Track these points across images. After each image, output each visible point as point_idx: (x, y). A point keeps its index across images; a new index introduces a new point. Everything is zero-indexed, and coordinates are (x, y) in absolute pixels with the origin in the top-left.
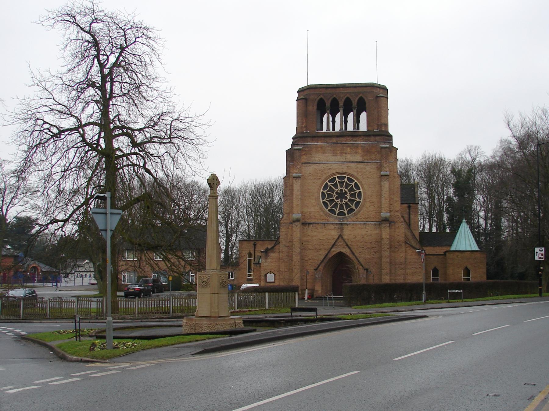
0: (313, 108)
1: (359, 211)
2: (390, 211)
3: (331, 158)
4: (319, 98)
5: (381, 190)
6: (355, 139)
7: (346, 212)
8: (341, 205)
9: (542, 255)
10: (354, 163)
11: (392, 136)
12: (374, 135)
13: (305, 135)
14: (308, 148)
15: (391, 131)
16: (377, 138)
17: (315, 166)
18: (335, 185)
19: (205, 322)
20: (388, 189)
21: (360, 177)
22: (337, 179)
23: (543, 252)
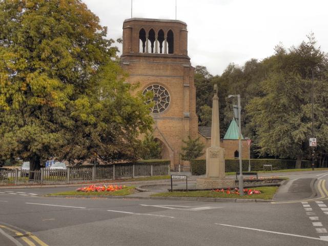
0: (136, 34)
1: (168, 110)
6: (166, 59)
9: (315, 143)
12: (179, 58)
13: (131, 54)
14: (133, 64)
15: (190, 54)
16: (182, 60)
19: (210, 195)
21: (168, 86)
23: (315, 141)
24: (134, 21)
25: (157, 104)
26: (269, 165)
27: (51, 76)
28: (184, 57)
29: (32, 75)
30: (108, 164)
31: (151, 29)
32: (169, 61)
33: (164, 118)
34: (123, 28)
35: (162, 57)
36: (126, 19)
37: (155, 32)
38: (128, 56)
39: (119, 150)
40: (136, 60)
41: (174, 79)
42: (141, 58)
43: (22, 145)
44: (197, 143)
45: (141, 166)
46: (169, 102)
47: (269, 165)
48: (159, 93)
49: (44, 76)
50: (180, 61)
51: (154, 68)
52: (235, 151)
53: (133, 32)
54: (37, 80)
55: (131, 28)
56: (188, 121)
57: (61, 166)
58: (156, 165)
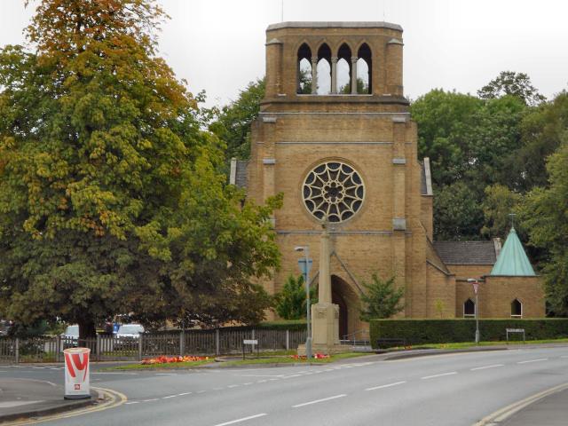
12: (383, 103)
13: (280, 100)
14: (284, 119)
24: (286, 28)
25: (336, 202)
26: (517, 330)
27: (104, 187)
28: (395, 100)
29: (76, 185)
30: (208, 328)
31: (322, 43)
32: (361, 111)
33: (352, 234)
34: (266, 45)
35: (345, 103)
36: (270, 23)
37: (332, 49)
38: (273, 103)
39: (217, 302)
40: (290, 112)
41: (372, 148)
42: (301, 106)
43: (60, 295)
44: (389, 289)
45: (267, 333)
46: (361, 197)
47: (517, 330)
48: (341, 180)
49: (94, 186)
50: (386, 110)
51: (331, 127)
52: (513, 300)
53: (284, 51)
54: (85, 193)
55: (281, 44)
56: (403, 237)
57: (133, 330)
58: (296, 330)
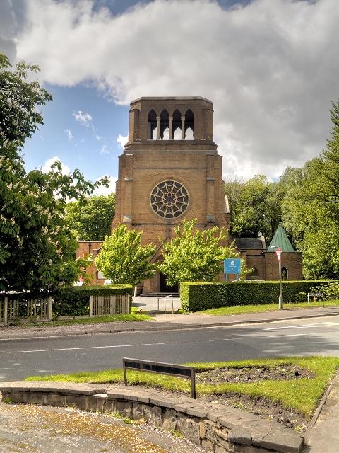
0: (144, 118)
2: (215, 214)
3: (160, 164)
4: (151, 109)
5: (206, 195)
7: (173, 214)
8: (174, 207)
10: (184, 171)
11: (216, 146)
12: (200, 144)
14: (315, 288)
17: (146, 172)
18: (164, 190)
20: (213, 194)
22: (166, 184)
